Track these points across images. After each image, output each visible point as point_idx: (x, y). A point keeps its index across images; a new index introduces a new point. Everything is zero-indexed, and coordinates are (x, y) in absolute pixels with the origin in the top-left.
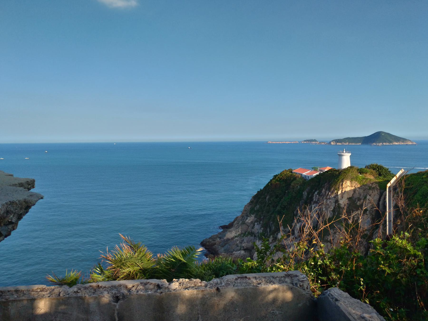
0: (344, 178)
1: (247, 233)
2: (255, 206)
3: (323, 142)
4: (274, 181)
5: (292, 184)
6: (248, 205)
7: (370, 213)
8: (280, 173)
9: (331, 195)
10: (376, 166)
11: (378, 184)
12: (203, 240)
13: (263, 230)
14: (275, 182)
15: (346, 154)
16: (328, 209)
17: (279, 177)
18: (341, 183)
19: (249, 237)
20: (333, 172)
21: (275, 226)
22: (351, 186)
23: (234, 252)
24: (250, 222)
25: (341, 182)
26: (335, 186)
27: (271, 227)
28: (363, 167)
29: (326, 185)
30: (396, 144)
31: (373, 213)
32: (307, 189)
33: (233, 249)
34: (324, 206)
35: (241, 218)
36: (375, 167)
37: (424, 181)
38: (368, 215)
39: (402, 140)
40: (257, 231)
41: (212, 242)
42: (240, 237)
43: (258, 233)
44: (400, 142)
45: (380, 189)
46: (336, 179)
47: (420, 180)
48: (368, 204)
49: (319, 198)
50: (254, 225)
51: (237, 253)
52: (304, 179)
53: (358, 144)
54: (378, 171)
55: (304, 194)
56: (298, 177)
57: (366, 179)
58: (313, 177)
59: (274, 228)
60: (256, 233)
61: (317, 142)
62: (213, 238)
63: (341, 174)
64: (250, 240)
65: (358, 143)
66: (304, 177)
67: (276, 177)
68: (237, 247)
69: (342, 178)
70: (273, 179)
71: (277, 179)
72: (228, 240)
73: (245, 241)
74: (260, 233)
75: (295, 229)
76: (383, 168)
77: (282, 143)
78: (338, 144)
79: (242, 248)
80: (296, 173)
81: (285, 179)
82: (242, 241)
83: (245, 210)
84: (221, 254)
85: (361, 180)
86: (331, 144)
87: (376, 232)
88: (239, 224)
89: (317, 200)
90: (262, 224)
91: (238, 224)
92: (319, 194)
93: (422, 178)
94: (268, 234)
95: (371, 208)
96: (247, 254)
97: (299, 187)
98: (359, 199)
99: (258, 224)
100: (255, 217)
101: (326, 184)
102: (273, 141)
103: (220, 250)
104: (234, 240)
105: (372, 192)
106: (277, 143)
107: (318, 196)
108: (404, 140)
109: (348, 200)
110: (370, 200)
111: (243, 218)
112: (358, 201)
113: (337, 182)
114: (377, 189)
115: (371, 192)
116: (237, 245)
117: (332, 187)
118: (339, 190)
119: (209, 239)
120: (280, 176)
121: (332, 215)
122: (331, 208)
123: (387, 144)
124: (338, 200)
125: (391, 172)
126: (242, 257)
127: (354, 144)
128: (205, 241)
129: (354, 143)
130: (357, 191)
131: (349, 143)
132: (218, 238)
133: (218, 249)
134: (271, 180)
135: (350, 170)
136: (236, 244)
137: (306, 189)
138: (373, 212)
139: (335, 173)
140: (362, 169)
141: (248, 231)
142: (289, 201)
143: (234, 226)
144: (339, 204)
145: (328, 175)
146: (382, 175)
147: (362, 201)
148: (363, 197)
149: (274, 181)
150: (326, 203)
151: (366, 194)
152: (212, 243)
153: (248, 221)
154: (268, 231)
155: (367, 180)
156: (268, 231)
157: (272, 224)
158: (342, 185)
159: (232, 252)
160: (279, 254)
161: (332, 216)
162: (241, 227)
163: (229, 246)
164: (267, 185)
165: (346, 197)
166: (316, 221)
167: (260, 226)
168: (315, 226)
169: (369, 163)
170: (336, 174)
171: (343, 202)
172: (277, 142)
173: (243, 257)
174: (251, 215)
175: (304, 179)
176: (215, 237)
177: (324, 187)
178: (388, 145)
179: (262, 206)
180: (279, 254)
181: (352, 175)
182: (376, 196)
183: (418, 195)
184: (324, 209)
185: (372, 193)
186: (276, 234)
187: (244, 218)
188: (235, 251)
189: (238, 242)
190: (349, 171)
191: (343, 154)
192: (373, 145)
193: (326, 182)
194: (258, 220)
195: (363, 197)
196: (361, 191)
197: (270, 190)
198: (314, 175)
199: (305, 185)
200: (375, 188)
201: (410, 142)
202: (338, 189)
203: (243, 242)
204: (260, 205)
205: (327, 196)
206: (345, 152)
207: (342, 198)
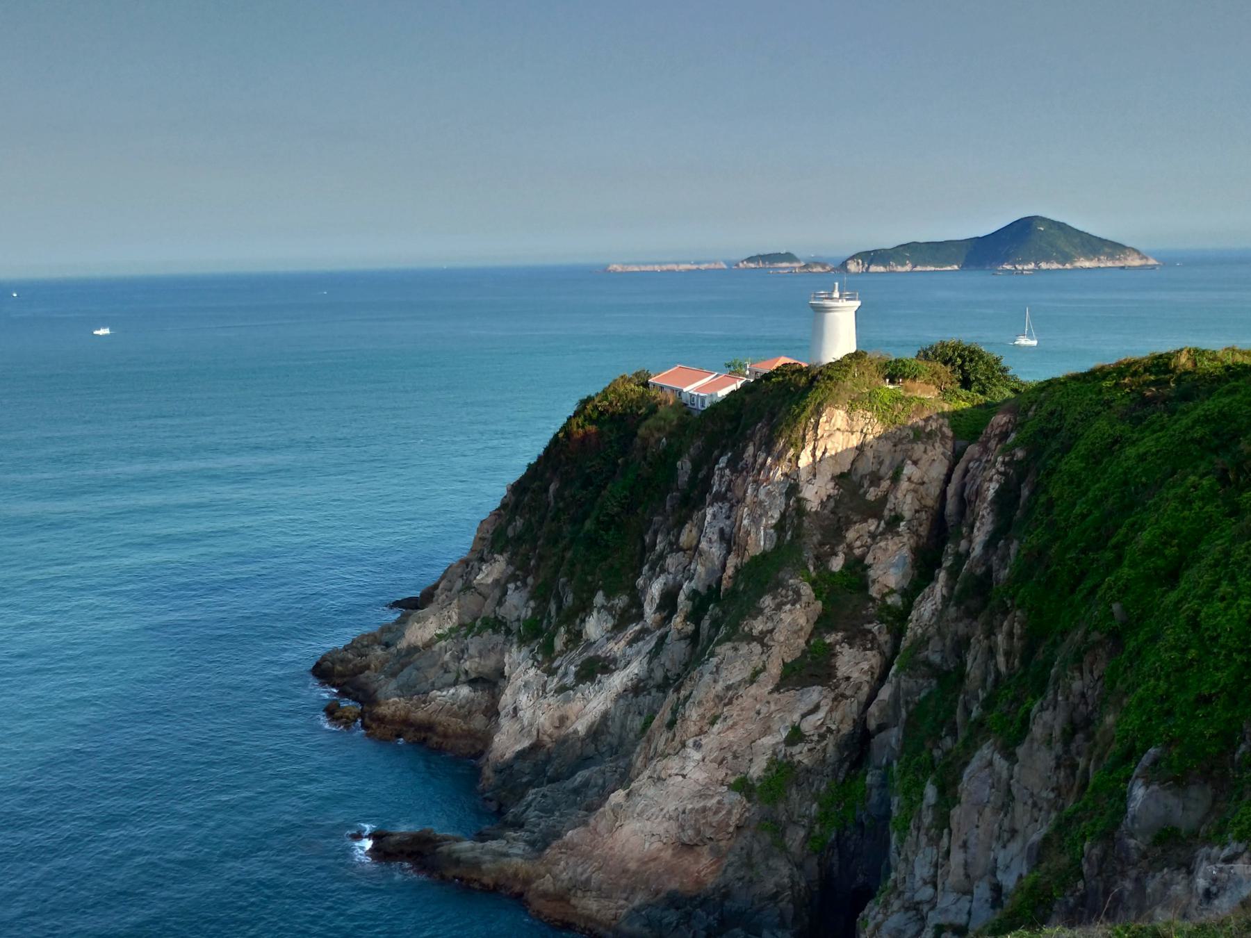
0: (825, 399)
1: (478, 623)
2: (509, 522)
3: (817, 263)
4: (577, 424)
5: (642, 431)
6: (494, 517)
7: (908, 529)
8: (604, 391)
9: (773, 467)
10: (955, 349)
11: (948, 418)
12: (322, 652)
13: (533, 609)
14: (583, 427)
15: (840, 303)
16: (762, 520)
17: (596, 407)
18: (812, 420)
19: (485, 635)
20: (787, 378)
21: (574, 593)
22: (847, 431)
23: (435, 691)
24: (490, 580)
25: (813, 414)
26: (789, 432)
27: (562, 594)
28: (909, 355)
29: (759, 430)
30: (1087, 264)
31: (921, 529)
32: (691, 450)
33: (430, 681)
34: (746, 509)
35: (459, 570)
36: (950, 353)
37: (1102, 402)
38: (902, 535)
39: (1107, 250)
40: (516, 614)
41: (354, 662)
42: (456, 637)
43: (518, 620)
44: (1102, 257)
45: (954, 438)
46: (797, 404)
47: (1091, 399)
48: (905, 496)
49: (731, 480)
50: (505, 593)
51: (444, 696)
52: (685, 408)
53: (949, 268)
54: (961, 367)
55: (680, 468)
56: (666, 402)
57: (907, 400)
58: (719, 401)
59: (574, 599)
60: (513, 620)
61: (796, 265)
62: (359, 646)
63: (815, 384)
64: (490, 647)
65: (946, 266)
66: (689, 398)
67: (585, 408)
68: (447, 675)
69: (818, 400)
70: (577, 414)
71: (590, 415)
72: (412, 650)
73: (473, 650)
74: (525, 620)
75: (645, 600)
76: (981, 357)
77: (662, 271)
78: (873, 269)
79: (463, 678)
80: (662, 388)
81: (620, 414)
82: (462, 651)
83: (480, 538)
84: (387, 704)
85: (889, 407)
86: (847, 271)
87: (923, 598)
88: (452, 592)
89: (723, 489)
90: (532, 587)
91: (450, 590)
92: (732, 464)
93: (1096, 389)
94: (553, 621)
95: (917, 511)
96: (482, 698)
97: (664, 440)
98: (875, 479)
99: (517, 588)
100: (509, 563)
101: (760, 424)
102: (628, 264)
103: (384, 688)
104: (434, 649)
105: (926, 448)
106: (643, 268)
107: (727, 472)
108: (1115, 248)
109: (835, 485)
110: (912, 479)
111: (469, 569)
112: (872, 484)
113: (799, 415)
114: (944, 436)
115: (919, 448)
116: (445, 666)
117: (780, 435)
118: (803, 448)
119: (346, 650)
120: (599, 402)
121: (774, 543)
122: (772, 516)
123: (1055, 266)
124: (798, 485)
125: (1011, 372)
126: (463, 707)
127: (933, 269)
128: (330, 659)
129: (935, 267)
130: (871, 447)
131: (915, 266)
132: (376, 647)
133: (376, 685)
134: (570, 419)
135: (850, 366)
136: (440, 663)
137: (689, 447)
138: (921, 525)
139: (795, 380)
140: (900, 364)
141: (482, 617)
142: (626, 497)
143: (437, 600)
144: (800, 501)
145: (771, 391)
146: (975, 383)
147: (885, 484)
148: (891, 469)
149: (577, 424)
150: (756, 499)
151: (900, 458)
152: (355, 665)
153: (482, 579)
154: (553, 613)
155: (911, 403)
156: (553, 613)
157: (564, 585)
158: (817, 428)
159: (426, 693)
160: (587, 692)
161: (773, 547)
162: (459, 600)
163: (415, 672)
164: (555, 440)
165: (828, 473)
166: (716, 568)
167: (525, 594)
168: (714, 586)
169: (934, 336)
170: (796, 386)
171: (816, 493)
172: (646, 264)
173: (466, 709)
174: (495, 556)
175: (684, 407)
176: (365, 643)
177: (751, 438)
178: (1059, 269)
179: (533, 519)
180: (587, 692)
181: (856, 385)
182: (936, 464)
183: (1073, 456)
184: (745, 522)
185: (925, 452)
186: (578, 621)
187: (472, 568)
188: (439, 690)
189: (447, 657)
190: (846, 371)
191: (828, 303)
192: (999, 271)
193: (760, 419)
194: (517, 573)
195: (891, 469)
196: (886, 447)
197: (562, 457)
198: (723, 393)
199: (687, 432)
200: (936, 435)
201: (1136, 256)
202: (800, 444)
203: (466, 656)
204: (527, 516)
205: (759, 473)
206: (836, 295)
207: (815, 475)
